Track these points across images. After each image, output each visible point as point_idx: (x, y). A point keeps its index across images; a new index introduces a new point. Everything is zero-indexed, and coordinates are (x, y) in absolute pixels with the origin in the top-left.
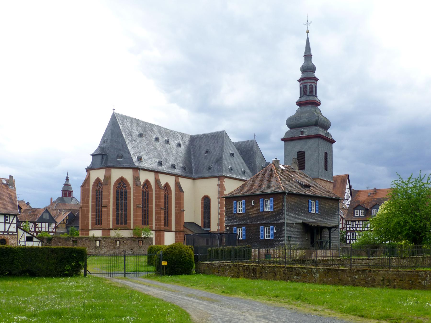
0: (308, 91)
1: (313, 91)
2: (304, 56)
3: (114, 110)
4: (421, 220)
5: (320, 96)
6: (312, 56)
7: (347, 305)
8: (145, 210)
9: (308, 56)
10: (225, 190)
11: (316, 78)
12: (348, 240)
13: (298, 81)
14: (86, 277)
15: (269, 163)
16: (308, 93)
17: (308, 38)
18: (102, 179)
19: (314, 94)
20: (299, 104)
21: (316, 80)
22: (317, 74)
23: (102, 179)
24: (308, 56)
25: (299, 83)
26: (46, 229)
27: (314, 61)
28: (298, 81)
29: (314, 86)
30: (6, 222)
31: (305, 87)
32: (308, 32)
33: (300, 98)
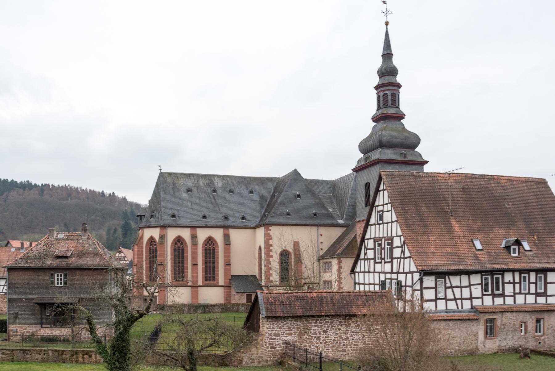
1: (395, 100)
2: (382, 56)
3: (161, 170)
5: (404, 106)
6: (393, 55)
7: (34, 300)
9: (387, 55)
11: (399, 84)
13: (374, 88)
15: (83, 190)
16: (390, 104)
17: (387, 33)
18: (157, 238)
20: (376, 119)
21: (399, 86)
23: (157, 238)
24: (387, 55)
27: (396, 61)
28: (374, 88)
29: (389, 93)
30: (496, 292)
31: (385, 95)
32: (387, 24)
33: (377, 110)
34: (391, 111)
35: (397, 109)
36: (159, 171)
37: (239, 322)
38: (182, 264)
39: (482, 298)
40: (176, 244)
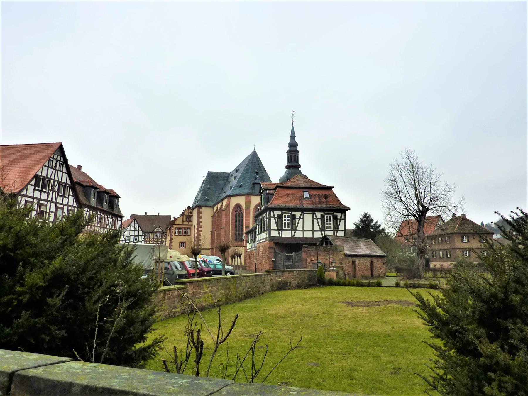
0: (293, 159)
4: (226, 261)
5: (300, 162)
6: (299, 152)
8: (238, 236)
9: (293, 137)
10: (201, 214)
12: (54, 158)
14: (365, 213)
16: (293, 161)
19: (297, 161)
21: (299, 152)
22: (299, 148)
24: (293, 137)
25: (287, 154)
26: (315, 229)
27: (297, 140)
32: (293, 122)
34: (294, 164)
35: (297, 163)
36: (253, 150)
37: (15, 296)
38: (241, 222)
39: (130, 235)
40: (237, 211)
